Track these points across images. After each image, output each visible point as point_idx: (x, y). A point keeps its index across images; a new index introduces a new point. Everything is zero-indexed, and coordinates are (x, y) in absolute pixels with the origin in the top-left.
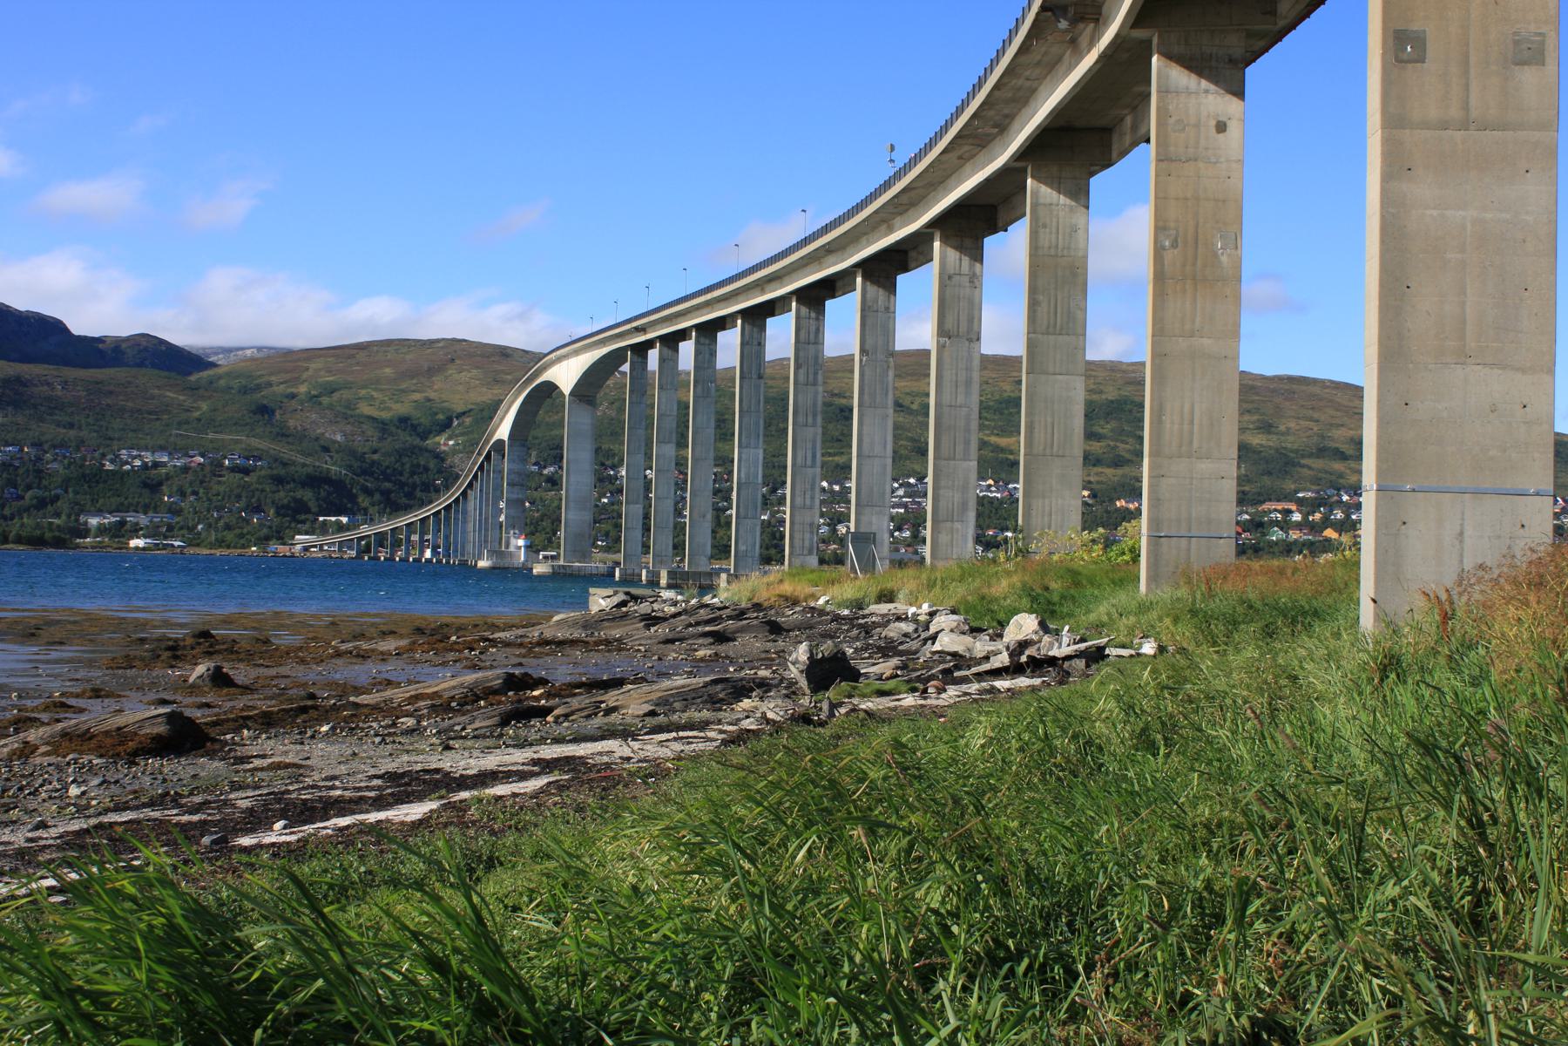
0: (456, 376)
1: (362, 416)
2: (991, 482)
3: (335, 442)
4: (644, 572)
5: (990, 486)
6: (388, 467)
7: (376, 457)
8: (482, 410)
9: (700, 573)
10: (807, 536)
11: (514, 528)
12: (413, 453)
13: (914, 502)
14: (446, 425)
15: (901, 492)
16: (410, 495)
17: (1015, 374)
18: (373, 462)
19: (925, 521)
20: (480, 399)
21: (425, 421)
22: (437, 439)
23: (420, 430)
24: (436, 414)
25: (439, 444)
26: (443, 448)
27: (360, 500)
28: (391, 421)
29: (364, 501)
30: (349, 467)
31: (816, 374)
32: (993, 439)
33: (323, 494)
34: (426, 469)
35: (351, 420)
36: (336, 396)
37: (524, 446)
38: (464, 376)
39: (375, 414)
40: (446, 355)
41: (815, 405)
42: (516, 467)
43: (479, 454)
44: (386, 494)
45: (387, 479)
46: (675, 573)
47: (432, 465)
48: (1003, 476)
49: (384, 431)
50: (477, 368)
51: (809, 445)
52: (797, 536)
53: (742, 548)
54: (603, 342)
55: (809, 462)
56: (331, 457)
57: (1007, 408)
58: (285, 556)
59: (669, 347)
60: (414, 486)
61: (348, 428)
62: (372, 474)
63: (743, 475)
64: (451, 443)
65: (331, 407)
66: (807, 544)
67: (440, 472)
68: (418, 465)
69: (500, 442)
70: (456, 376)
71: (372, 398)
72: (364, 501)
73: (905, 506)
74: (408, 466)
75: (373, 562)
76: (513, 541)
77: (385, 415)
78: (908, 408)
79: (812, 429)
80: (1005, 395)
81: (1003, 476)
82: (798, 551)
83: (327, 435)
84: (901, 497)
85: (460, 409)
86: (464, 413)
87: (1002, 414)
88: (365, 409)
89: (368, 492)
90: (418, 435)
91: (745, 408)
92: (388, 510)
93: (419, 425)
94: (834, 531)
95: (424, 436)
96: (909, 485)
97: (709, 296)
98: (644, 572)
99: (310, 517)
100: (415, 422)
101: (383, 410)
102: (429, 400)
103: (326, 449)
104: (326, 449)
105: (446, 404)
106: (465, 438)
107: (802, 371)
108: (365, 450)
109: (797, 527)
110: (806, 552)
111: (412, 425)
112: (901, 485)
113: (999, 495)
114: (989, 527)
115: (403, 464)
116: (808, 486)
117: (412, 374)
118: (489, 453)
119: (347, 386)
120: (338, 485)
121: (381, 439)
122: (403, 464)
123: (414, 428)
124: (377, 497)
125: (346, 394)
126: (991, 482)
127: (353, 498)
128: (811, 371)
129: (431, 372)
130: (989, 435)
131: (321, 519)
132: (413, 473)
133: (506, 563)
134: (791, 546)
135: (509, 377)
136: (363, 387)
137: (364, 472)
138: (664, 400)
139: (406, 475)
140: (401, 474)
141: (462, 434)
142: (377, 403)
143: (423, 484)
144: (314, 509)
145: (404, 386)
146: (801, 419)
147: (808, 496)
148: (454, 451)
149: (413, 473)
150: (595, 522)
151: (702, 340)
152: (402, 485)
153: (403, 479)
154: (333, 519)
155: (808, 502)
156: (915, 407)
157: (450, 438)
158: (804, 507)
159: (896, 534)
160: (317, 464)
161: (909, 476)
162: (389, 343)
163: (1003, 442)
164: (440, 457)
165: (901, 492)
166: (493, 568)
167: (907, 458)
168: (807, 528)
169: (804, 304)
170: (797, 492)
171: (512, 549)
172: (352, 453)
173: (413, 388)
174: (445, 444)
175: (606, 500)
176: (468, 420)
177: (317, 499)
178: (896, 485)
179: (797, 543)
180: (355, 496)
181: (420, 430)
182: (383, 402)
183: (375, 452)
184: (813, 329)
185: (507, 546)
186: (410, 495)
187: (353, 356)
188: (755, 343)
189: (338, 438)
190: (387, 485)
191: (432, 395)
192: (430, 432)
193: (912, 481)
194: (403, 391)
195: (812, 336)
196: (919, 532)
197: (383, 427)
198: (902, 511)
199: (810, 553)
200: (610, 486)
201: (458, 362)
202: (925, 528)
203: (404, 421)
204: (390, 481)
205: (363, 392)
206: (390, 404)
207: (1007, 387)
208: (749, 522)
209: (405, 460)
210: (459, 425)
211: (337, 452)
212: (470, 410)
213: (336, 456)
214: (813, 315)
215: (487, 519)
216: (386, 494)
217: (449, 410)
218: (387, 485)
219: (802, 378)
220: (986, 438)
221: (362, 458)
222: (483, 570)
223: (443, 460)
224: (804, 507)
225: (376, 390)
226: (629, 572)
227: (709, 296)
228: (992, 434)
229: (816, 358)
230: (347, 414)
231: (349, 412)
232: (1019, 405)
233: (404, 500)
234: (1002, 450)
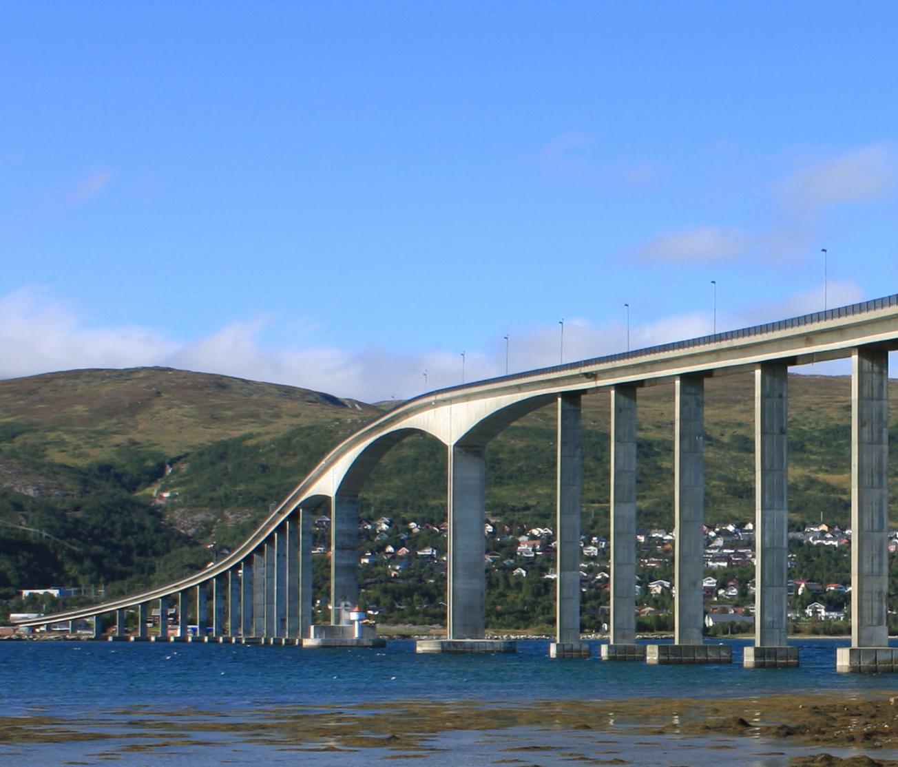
0: (164, 413)
1: (52, 465)
2: (824, 528)
3: (27, 497)
4: (272, 639)
5: (823, 532)
6: (95, 527)
7: (79, 515)
8: (201, 454)
9: (694, 647)
10: (876, 605)
11: (345, 599)
12: (123, 509)
13: (737, 554)
14: (157, 474)
15: (720, 542)
16: (126, 560)
17: (842, 398)
18: (77, 522)
19: (753, 576)
20: (197, 441)
21: (131, 469)
22: (148, 490)
23: (126, 480)
24: (144, 460)
25: (151, 496)
26: (159, 502)
27: (67, 568)
28: (90, 470)
29: (72, 569)
30: (50, 528)
31: (880, 431)
32: (821, 476)
33: (23, 562)
34: (142, 528)
35: (44, 470)
36: (19, 441)
37: (354, 502)
38: (175, 413)
39: (69, 461)
40: (150, 387)
41: (880, 464)
42: (344, 527)
43: (281, 512)
44: (97, 559)
45: (96, 541)
46: (667, 648)
47: (148, 522)
48: (837, 519)
49: (84, 482)
50: (190, 402)
51: (876, 508)
52: (866, 605)
53: (768, 619)
54: (519, 388)
55: (876, 526)
56: (26, 517)
57: (835, 439)
58: (10, 639)
59: (625, 395)
60: (129, 549)
61: (42, 481)
62: (77, 536)
63: (767, 539)
64: (166, 495)
65: (14, 454)
66: (876, 613)
67: (158, 531)
68: (132, 524)
69: (320, 503)
70: (164, 413)
71: (63, 442)
72: (72, 569)
73: (727, 558)
74: (119, 525)
75: (118, 643)
76: (344, 615)
77: (81, 463)
78: (718, 441)
79: (877, 492)
80: (832, 423)
81: (837, 519)
82: (867, 621)
83: (16, 489)
84: (722, 548)
85: (173, 453)
86: (179, 459)
87: (829, 446)
88: (56, 456)
89: (77, 559)
90: (123, 486)
91: (768, 467)
92: (102, 579)
93: (123, 474)
94: (648, 590)
95: (133, 486)
96: (727, 533)
97: (725, 344)
98: (272, 639)
99: (11, 590)
100: (119, 471)
101: (80, 456)
102: (134, 443)
103: (18, 507)
104: (18, 507)
105: (155, 448)
106: (183, 489)
107: (865, 429)
108: (65, 506)
109: (865, 596)
110: (875, 622)
111: (116, 475)
112: (718, 534)
113: (836, 543)
114: (829, 582)
115: (113, 523)
116: (875, 552)
117: (111, 411)
118: (296, 510)
119: (31, 428)
120: (38, 550)
121: (84, 492)
122: (113, 523)
123: (118, 477)
124: (88, 563)
125: (31, 439)
126: (824, 528)
127: (59, 567)
128: (876, 428)
129: (135, 408)
130: (816, 472)
131: (26, 593)
132: (125, 534)
133: (336, 640)
134: (860, 616)
135: (230, 413)
136: (52, 429)
137: (68, 534)
138: (621, 454)
139: (118, 536)
140: (111, 534)
141: (179, 484)
142: (70, 448)
143: (139, 546)
144: (15, 581)
145: (101, 427)
146: (867, 480)
147: (876, 561)
148: (174, 507)
149: (125, 534)
150: (360, 588)
151: (688, 389)
152: (115, 548)
153: (114, 541)
154: (41, 592)
155: (876, 569)
156: (726, 439)
157: (164, 489)
158: (872, 574)
159: (721, 592)
160: (10, 525)
161: (727, 523)
162: (77, 374)
163: (833, 479)
164: (156, 513)
165: (720, 542)
166: (323, 647)
167: (722, 501)
168: (876, 597)
169: (867, 357)
170: (865, 559)
171: (343, 624)
172: (51, 510)
173: (114, 429)
174: (161, 497)
175: (366, 561)
176: (184, 467)
177: (17, 569)
178: (712, 534)
179: (866, 613)
180: (61, 564)
181: (126, 480)
182: (77, 447)
183: (77, 508)
184: (876, 383)
185: (338, 620)
186: (126, 560)
187: (33, 392)
188: (776, 395)
189: (31, 492)
190: (98, 549)
191: (138, 437)
192: (138, 482)
193: (731, 528)
194: (102, 433)
195: (876, 392)
196: (747, 589)
197: (86, 478)
198: (725, 564)
199: (880, 623)
200: (368, 544)
201: (165, 396)
202: (754, 584)
203: (105, 469)
204: (100, 544)
205: (52, 436)
206: (86, 449)
207: (834, 415)
208: (775, 590)
209: (116, 517)
210: (173, 473)
211: (33, 510)
212: (187, 455)
213: (31, 515)
214: (876, 369)
215: (294, 590)
216: (97, 559)
217: (161, 455)
218: (98, 549)
219: (866, 436)
220: (813, 476)
221: (62, 515)
222: (311, 649)
223: (160, 516)
224: (872, 574)
225: (66, 432)
226: (567, 647)
227: (725, 344)
228: (821, 470)
229: (880, 415)
230: (34, 462)
231: (39, 461)
232: (849, 436)
233: (119, 567)
234: (834, 489)
